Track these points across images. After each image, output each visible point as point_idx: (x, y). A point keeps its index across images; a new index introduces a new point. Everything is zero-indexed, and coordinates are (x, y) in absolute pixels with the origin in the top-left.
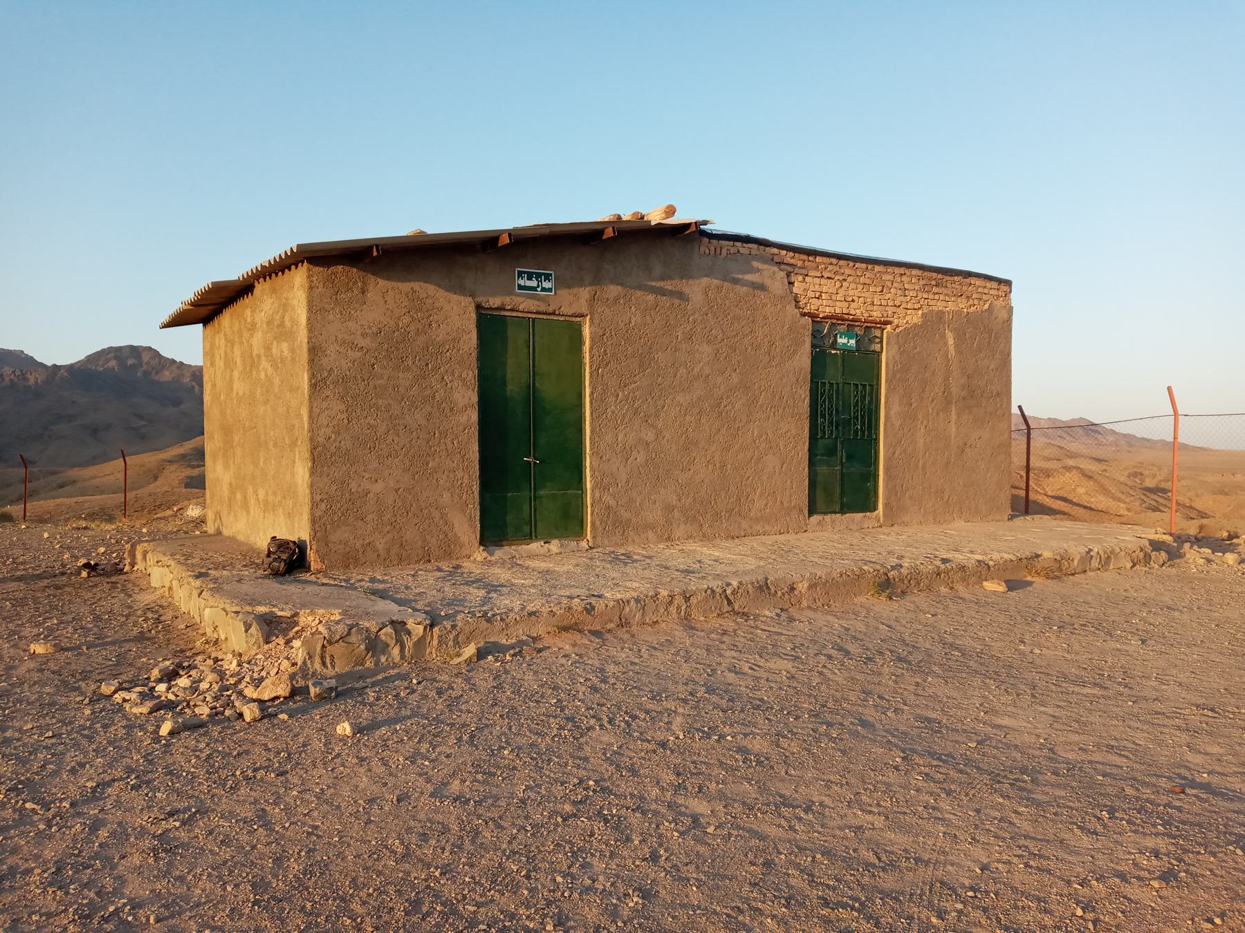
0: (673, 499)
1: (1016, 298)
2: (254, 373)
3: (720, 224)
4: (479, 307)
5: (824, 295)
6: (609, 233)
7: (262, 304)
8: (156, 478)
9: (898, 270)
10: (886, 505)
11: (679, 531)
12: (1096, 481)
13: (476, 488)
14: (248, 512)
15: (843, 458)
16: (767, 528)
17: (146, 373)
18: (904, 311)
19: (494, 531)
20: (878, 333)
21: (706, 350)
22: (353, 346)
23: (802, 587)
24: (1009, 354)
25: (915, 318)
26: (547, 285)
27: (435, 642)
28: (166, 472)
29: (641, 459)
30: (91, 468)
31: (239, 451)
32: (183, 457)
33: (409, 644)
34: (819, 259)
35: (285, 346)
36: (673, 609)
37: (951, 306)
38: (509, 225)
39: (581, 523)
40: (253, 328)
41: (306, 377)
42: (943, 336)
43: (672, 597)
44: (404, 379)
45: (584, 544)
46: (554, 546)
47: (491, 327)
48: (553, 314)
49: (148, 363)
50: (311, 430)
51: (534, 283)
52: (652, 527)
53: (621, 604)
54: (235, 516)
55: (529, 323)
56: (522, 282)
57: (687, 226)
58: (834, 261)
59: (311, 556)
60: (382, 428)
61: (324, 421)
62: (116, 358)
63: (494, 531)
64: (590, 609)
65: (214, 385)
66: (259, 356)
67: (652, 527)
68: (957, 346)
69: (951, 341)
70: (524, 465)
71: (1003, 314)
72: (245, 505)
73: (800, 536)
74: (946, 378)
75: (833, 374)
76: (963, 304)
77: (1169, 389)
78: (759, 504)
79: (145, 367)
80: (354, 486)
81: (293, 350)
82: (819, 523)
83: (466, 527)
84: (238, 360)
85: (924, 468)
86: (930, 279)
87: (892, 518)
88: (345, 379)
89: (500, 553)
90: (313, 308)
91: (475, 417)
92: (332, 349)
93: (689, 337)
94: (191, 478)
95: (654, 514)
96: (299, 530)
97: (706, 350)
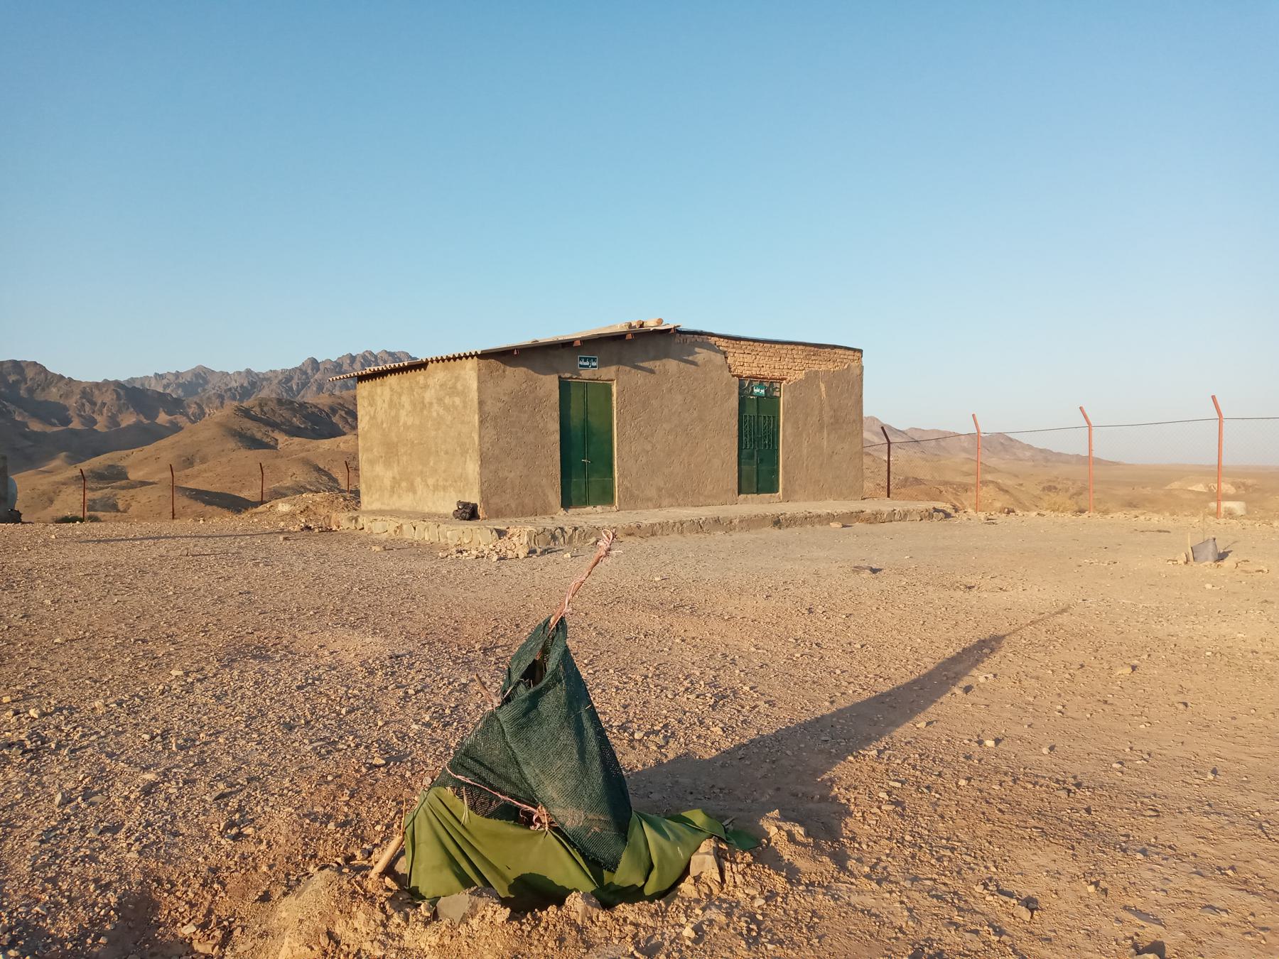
3: (686, 326)
5: (746, 364)
6: (629, 337)
7: (437, 375)
8: (51, 501)
9: (790, 347)
10: (784, 489)
12: (1011, 495)
14: (415, 492)
15: (758, 462)
17: (31, 391)
18: (793, 371)
19: (566, 503)
21: (679, 398)
22: (499, 400)
23: (736, 522)
25: (801, 376)
37: (823, 368)
40: (426, 387)
41: (477, 417)
42: (818, 386)
46: (599, 508)
47: (564, 386)
52: (649, 499)
53: (652, 525)
55: (585, 386)
57: (669, 330)
59: (480, 512)
61: (486, 439)
63: (566, 503)
64: (639, 527)
65: (373, 418)
66: (431, 404)
67: (649, 499)
70: (584, 466)
72: (412, 489)
74: (821, 410)
75: (751, 411)
76: (831, 366)
78: (710, 487)
81: (464, 402)
83: (555, 497)
87: (787, 498)
88: (496, 418)
89: (571, 511)
90: (481, 382)
91: (558, 437)
92: (489, 402)
93: (670, 390)
95: (652, 492)
96: (474, 498)
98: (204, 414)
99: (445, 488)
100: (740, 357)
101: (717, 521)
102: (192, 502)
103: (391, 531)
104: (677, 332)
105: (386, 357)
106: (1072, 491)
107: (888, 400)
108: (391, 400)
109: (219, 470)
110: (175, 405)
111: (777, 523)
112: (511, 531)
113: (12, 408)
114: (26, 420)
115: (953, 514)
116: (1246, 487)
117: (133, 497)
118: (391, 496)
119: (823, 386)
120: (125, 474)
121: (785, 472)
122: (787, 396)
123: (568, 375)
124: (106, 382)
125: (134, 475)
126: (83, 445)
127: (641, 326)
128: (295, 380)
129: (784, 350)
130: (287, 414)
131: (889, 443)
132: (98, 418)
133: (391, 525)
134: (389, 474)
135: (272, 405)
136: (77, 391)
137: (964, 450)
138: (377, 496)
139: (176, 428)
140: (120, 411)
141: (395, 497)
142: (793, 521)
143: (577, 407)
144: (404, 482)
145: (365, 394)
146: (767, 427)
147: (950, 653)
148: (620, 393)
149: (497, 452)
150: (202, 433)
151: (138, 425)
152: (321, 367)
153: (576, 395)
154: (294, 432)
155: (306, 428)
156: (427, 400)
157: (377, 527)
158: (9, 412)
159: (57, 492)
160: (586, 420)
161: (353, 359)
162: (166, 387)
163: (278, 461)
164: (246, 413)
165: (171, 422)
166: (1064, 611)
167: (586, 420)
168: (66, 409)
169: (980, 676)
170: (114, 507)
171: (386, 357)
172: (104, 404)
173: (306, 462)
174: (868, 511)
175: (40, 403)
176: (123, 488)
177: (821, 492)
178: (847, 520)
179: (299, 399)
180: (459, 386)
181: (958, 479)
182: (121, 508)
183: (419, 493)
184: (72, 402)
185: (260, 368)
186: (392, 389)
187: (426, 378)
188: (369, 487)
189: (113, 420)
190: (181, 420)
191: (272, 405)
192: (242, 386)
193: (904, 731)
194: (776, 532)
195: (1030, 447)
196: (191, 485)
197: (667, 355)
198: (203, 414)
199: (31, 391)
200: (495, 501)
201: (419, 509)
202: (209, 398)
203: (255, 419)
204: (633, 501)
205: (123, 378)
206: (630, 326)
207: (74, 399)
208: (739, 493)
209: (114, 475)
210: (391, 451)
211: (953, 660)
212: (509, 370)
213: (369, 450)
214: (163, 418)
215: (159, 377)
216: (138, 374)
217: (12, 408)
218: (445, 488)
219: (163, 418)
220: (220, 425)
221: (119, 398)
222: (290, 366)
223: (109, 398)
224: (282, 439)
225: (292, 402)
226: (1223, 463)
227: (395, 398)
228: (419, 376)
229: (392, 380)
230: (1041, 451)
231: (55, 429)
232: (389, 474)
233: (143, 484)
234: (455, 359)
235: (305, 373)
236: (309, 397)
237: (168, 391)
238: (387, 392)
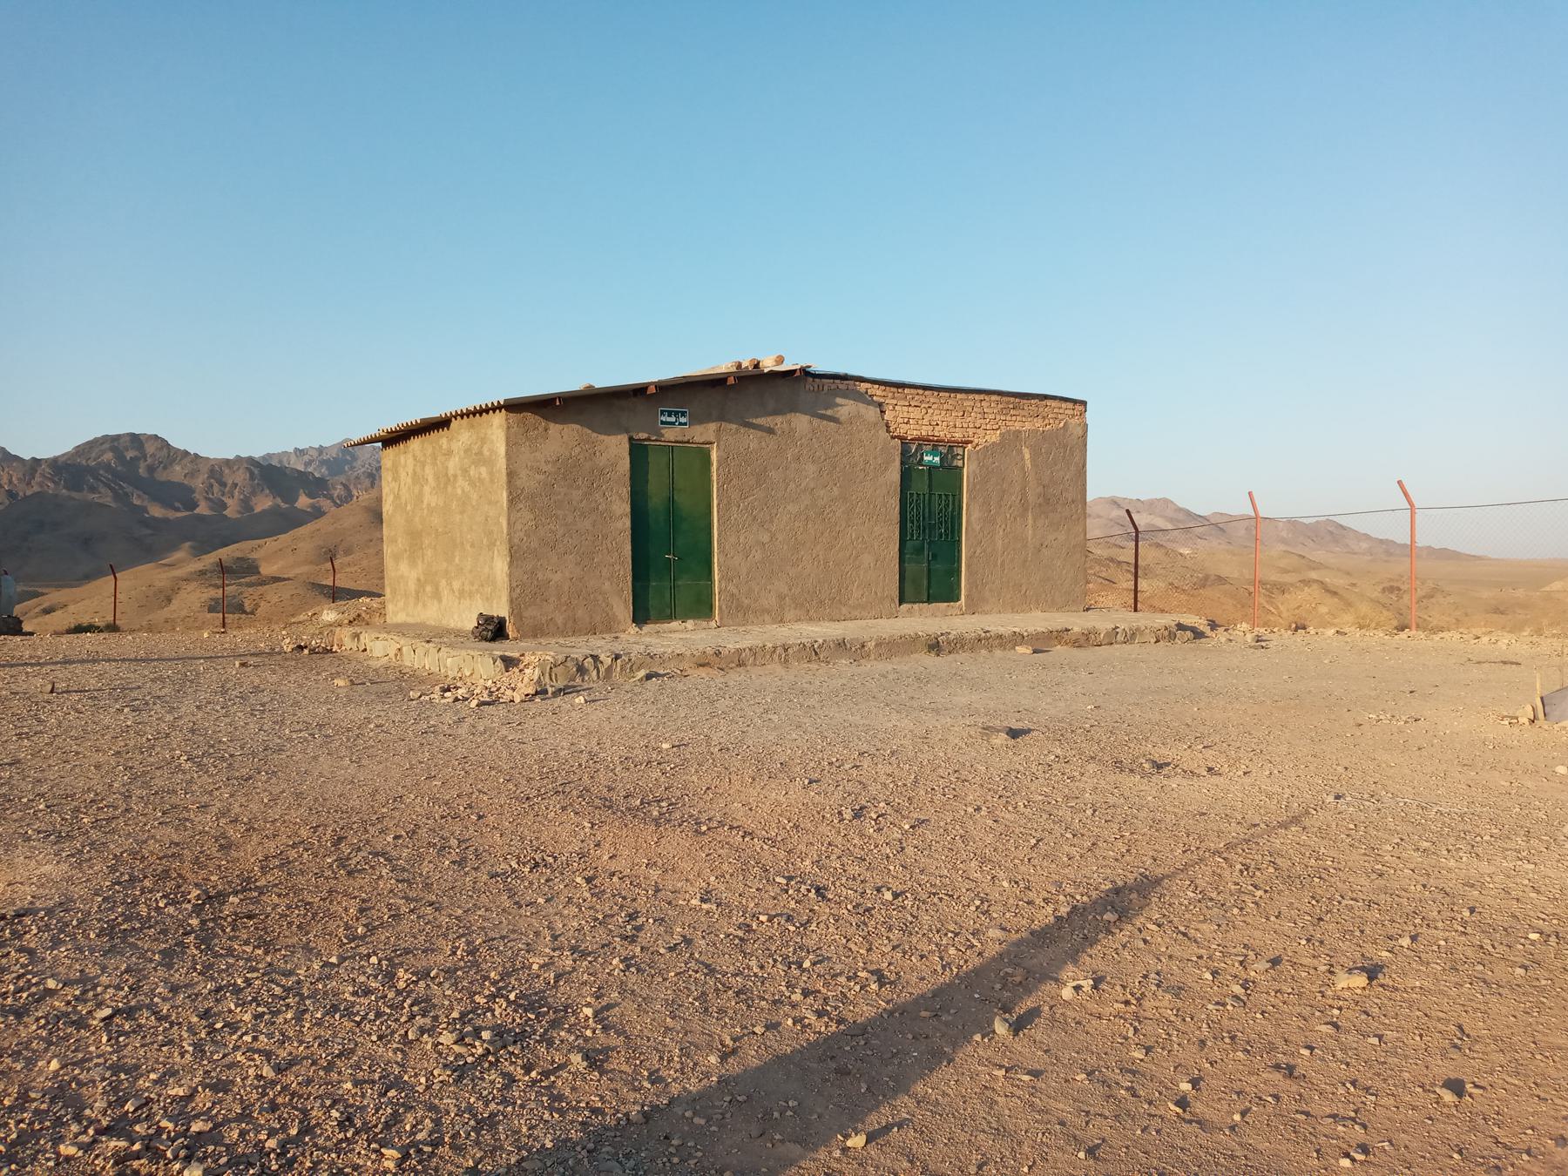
0: (785, 590)
2: (449, 489)
3: (819, 366)
4: (631, 439)
5: (912, 420)
6: (731, 381)
7: (461, 435)
8: (169, 600)
10: (967, 597)
11: (790, 615)
12: (1341, 598)
13: (629, 578)
14: (440, 601)
16: (864, 614)
19: (641, 616)
20: (960, 451)
21: (811, 469)
24: (1084, 465)
25: (994, 437)
26: (683, 420)
28: (183, 594)
29: (758, 556)
30: (67, 590)
31: (429, 553)
32: (202, 573)
33: (602, 670)
35: (483, 470)
36: (775, 657)
37: (1028, 426)
38: (655, 380)
39: (711, 607)
40: (449, 453)
41: (505, 495)
42: (1020, 452)
43: (775, 648)
44: (576, 494)
45: (713, 624)
46: (690, 624)
47: (638, 452)
49: (153, 455)
51: (673, 419)
53: (739, 651)
54: (424, 605)
55: (670, 450)
59: (510, 629)
60: (560, 533)
62: (114, 449)
64: (718, 654)
65: (397, 497)
66: (455, 476)
68: (1033, 460)
69: (1027, 456)
70: (667, 562)
72: (437, 595)
73: (892, 621)
75: (920, 486)
76: (1038, 423)
77: (1399, 482)
79: (149, 460)
80: (540, 576)
81: (491, 474)
84: (431, 478)
85: (1002, 564)
87: (972, 609)
89: (647, 628)
92: (523, 473)
94: (216, 600)
95: (769, 600)
96: (501, 610)
97: (811, 469)
98: (351, 496)
100: (902, 411)
101: (841, 644)
103: (392, 655)
104: (806, 373)
106: (1420, 593)
107: (1116, 472)
109: (365, 563)
110: (316, 486)
111: (935, 646)
112: (527, 659)
113: (129, 489)
114: (146, 503)
115: (1207, 630)
118: (416, 604)
120: (257, 568)
122: (974, 466)
123: (643, 435)
124: (239, 459)
125: (267, 570)
127: (757, 366)
129: (931, 397)
131: (1137, 531)
136: (205, 469)
137: (1284, 541)
139: (318, 513)
140: (253, 493)
142: (958, 644)
143: (654, 484)
144: (428, 587)
146: (943, 507)
147: (1045, 916)
151: (273, 512)
153: (656, 465)
156: (451, 472)
158: (126, 494)
159: (175, 590)
162: (308, 464)
165: (312, 506)
166: (1295, 820)
167: (671, 500)
169: (1071, 985)
170: (240, 609)
174: (1076, 629)
175: (162, 483)
177: (1023, 600)
178: (1041, 643)
180: (486, 453)
181: (1274, 577)
183: (444, 601)
184: (198, 483)
187: (450, 440)
189: (246, 504)
190: (325, 504)
193: (941, 1084)
194: (930, 660)
195: (1367, 537)
197: (794, 408)
198: (349, 497)
199: (151, 469)
200: (529, 613)
202: (357, 478)
204: (742, 612)
205: (257, 453)
206: (739, 365)
207: (200, 480)
208: (901, 602)
209: (246, 568)
211: (1042, 937)
212: (554, 428)
213: (394, 541)
214: (303, 502)
215: (299, 452)
217: (129, 489)
218: (471, 595)
219: (303, 502)
221: (252, 477)
223: (241, 477)
227: (418, 469)
228: (440, 438)
229: (415, 444)
230: (1381, 541)
231: (179, 515)
233: (276, 579)
234: (487, 411)
238: (410, 461)
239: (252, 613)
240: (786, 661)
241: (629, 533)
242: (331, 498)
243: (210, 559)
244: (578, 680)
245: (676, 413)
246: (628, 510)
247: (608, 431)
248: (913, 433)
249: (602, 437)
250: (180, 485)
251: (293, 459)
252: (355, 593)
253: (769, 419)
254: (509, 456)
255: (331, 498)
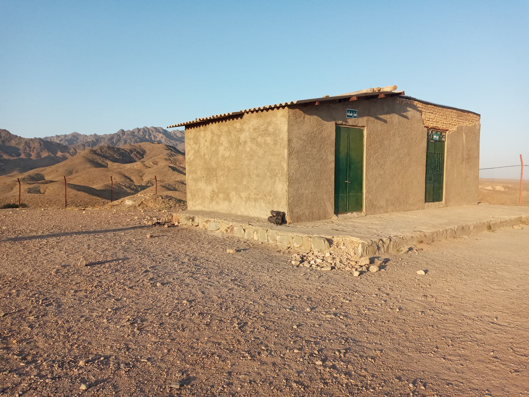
1: (482, 121)
4: (336, 124)
5: (433, 119)
7: (251, 122)
8: (12, 189)
10: (446, 199)
13: (333, 192)
14: (230, 201)
19: (337, 212)
22: (301, 139)
26: (355, 115)
27: (392, 247)
33: (385, 247)
34: (429, 106)
36: (443, 236)
40: (242, 130)
41: (286, 151)
47: (338, 129)
48: (356, 126)
50: (288, 171)
51: (351, 115)
52: (382, 207)
56: (348, 114)
58: (433, 106)
60: (308, 170)
61: (292, 167)
63: (337, 212)
65: (197, 152)
66: (245, 142)
67: (382, 207)
69: (464, 137)
71: (478, 127)
72: (228, 198)
74: (463, 152)
77: (521, 155)
82: (428, 206)
83: (330, 207)
86: (459, 114)
88: (298, 152)
89: (340, 215)
90: (290, 125)
92: (295, 140)
94: (30, 189)
95: (383, 203)
96: (283, 208)
98: (77, 152)
99: (255, 200)
102: (72, 190)
104: (399, 95)
105: (153, 129)
108: (212, 140)
109: (83, 176)
110: (64, 149)
116: (509, 188)
117: (47, 187)
119: (464, 135)
121: (446, 188)
124: (35, 139)
125: (47, 178)
126: (26, 165)
128: (115, 138)
130: (112, 153)
132: (32, 154)
133: (224, 226)
134: (209, 188)
135: (106, 149)
138: (200, 201)
139: (65, 158)
140: (41, 151)
141: (214, 203)
145: (191, 136)
148: (369, 135)
149: (298, 176)
150: (76, 160)
151: (48, 157)
152: (126, 133)
153: (344, 135)
154: (115, 160)
155: (120, 159)
157: (212, 226)
160: (348, 155)
161: (139, 130)
163: (108, 173)
164: (95, 152)
165: (63, 155)
167: (348, 155)
168: (19, 150)
171: (153, 129)
172: (34, 148)
173: (120, 173)
175: (8, 147)
176: (42, 183)
179: (116, 146)
180: (271, 129)
182: (42, 191)
183: (234, 202)
184: (21, 147)
185: (101, 133)
186: (213, 133)
188: (193, 196)
189: (38, 155)
190: (67, 155)
191: (106, 149)
192: (92, 141)
196: (71, 182)
201: (233, 212)
203: (98, 155)
204: (374, 208)
205: (42, 137)
206: (373, 91)
208: (426, 202)
209: (39, 178)
210: (210, 173)
212: (307, 117)
214: (59, 154)
215: (57, 137)
216: (49, 135)
219: (59, 154)
220: (84, 157)
221: (41, 145)
222: (113, 132)
223: (37, 145)
224: (110, 163)
225: (114, 148)
226: (523, 178)
227: (215, 138)
228: (237, 123)
232: (209, 188)
233: (51, 182)
234: (271, 108)
235: (119, 136)
236: (121, 146)
237: (61, 143)
239: (43, 193)
240: (447, 238)
241: (334, 170)
242: (69, 153)
243: (26, 175)
244: (377, 254)
245: (353, 111)
246: (334, 159)
247: (328, 119)
248: (431, 125)
249: (325, 122)
250: (14, 147)
251: (55, 139)
252: (175, 196)
253: (385, 116)
254: (289, 132)
255: (69, 153)
